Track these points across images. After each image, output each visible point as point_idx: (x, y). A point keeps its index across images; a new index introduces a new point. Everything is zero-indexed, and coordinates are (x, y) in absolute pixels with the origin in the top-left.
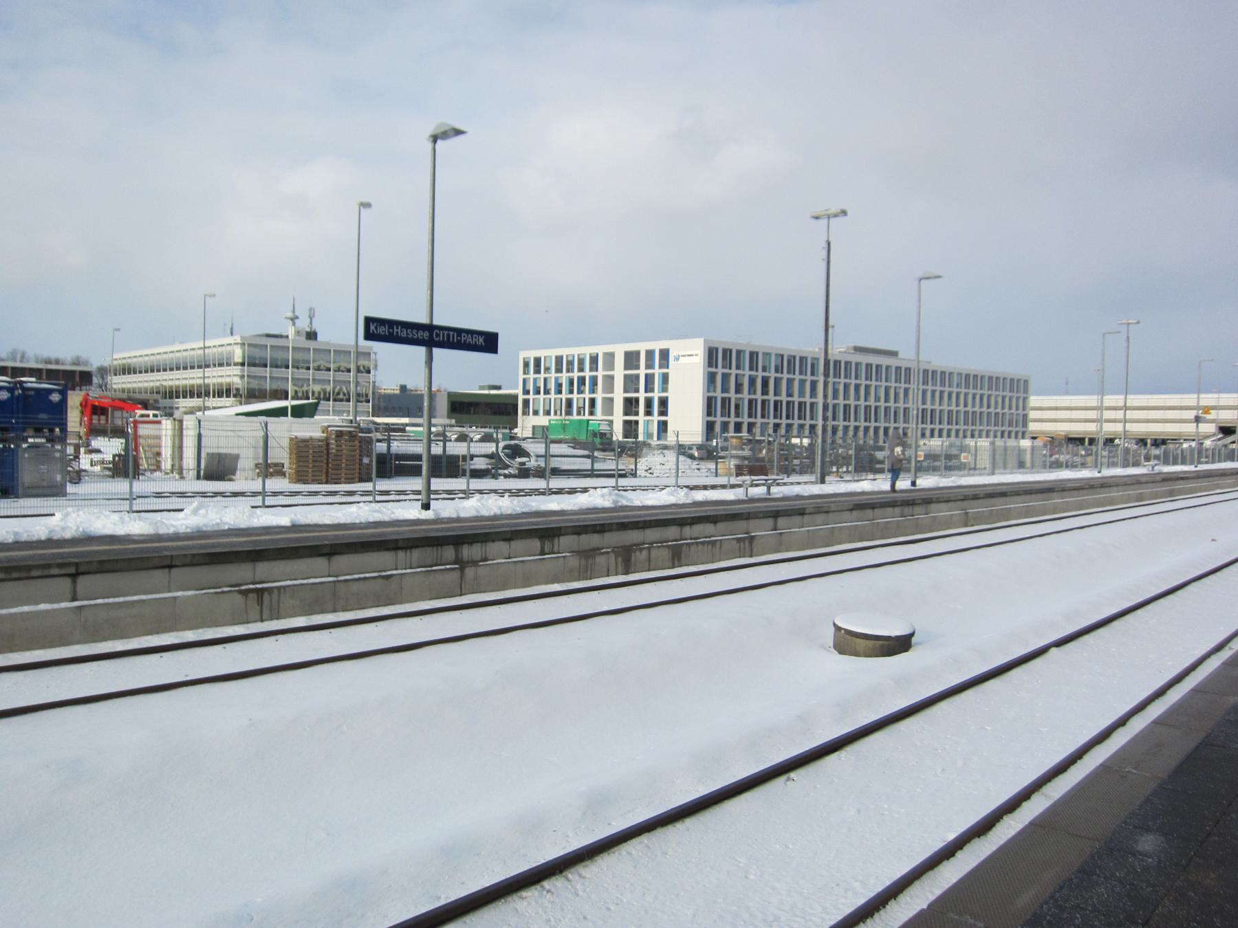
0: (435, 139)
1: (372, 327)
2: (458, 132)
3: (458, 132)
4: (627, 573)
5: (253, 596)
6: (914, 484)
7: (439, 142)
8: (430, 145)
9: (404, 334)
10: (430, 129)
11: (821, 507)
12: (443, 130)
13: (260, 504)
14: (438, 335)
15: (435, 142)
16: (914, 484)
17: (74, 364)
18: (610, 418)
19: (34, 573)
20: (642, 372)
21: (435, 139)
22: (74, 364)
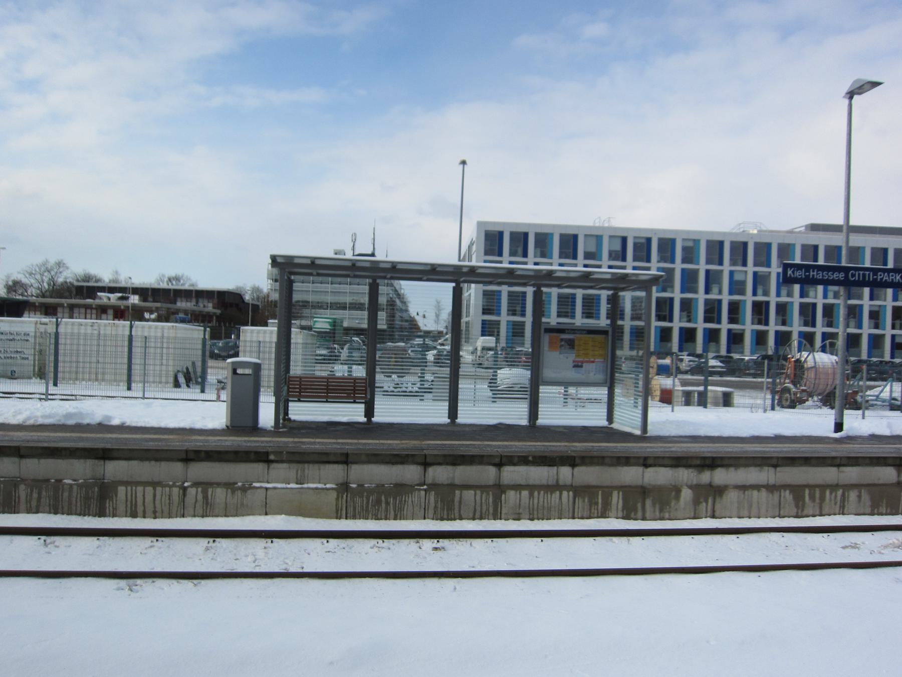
0: (851, 95)
1: (790, 272)
2: (875, 84)
3: (875, 84)
4: (101, 514)
5: (787, 495)
6: (839, 427)
7: (856, 97)
8: (847, 101)
9: (820, 277)
10: (846, 87)
11: (707, 459)
12: (858, 85)
13: (141, 395)
14: (853, 275)
15: (851, 98)
16: (839, 427)
17: (84, 281)
18: (487, 317)
19: (698, 462)
20: (702, 267)
21: (851, 95)
22: (84, 281)
